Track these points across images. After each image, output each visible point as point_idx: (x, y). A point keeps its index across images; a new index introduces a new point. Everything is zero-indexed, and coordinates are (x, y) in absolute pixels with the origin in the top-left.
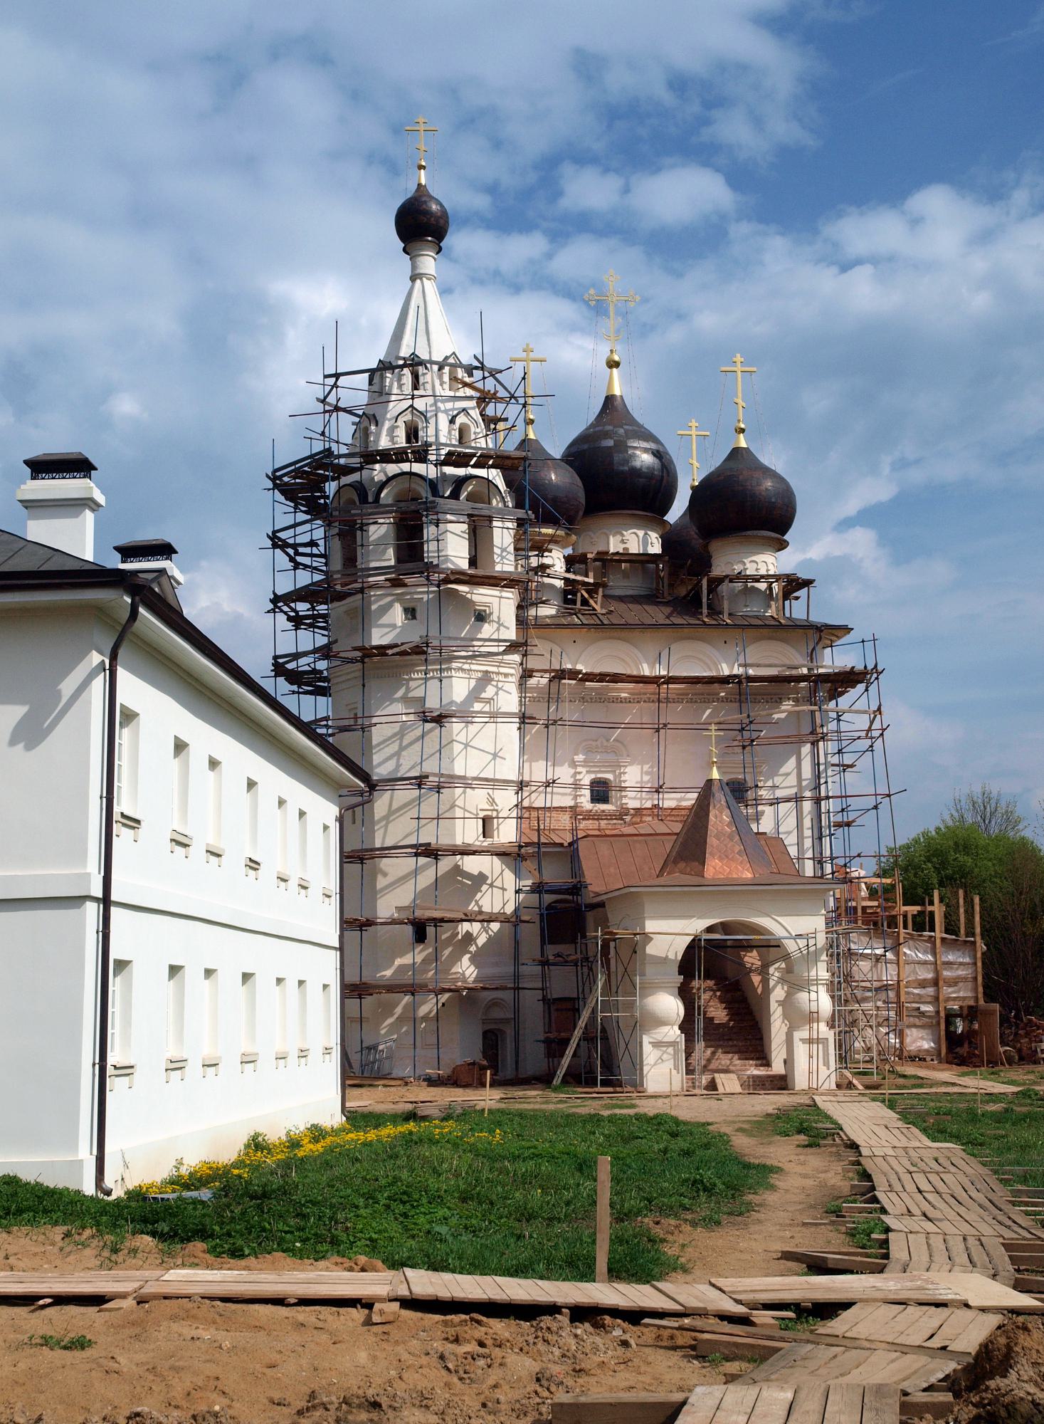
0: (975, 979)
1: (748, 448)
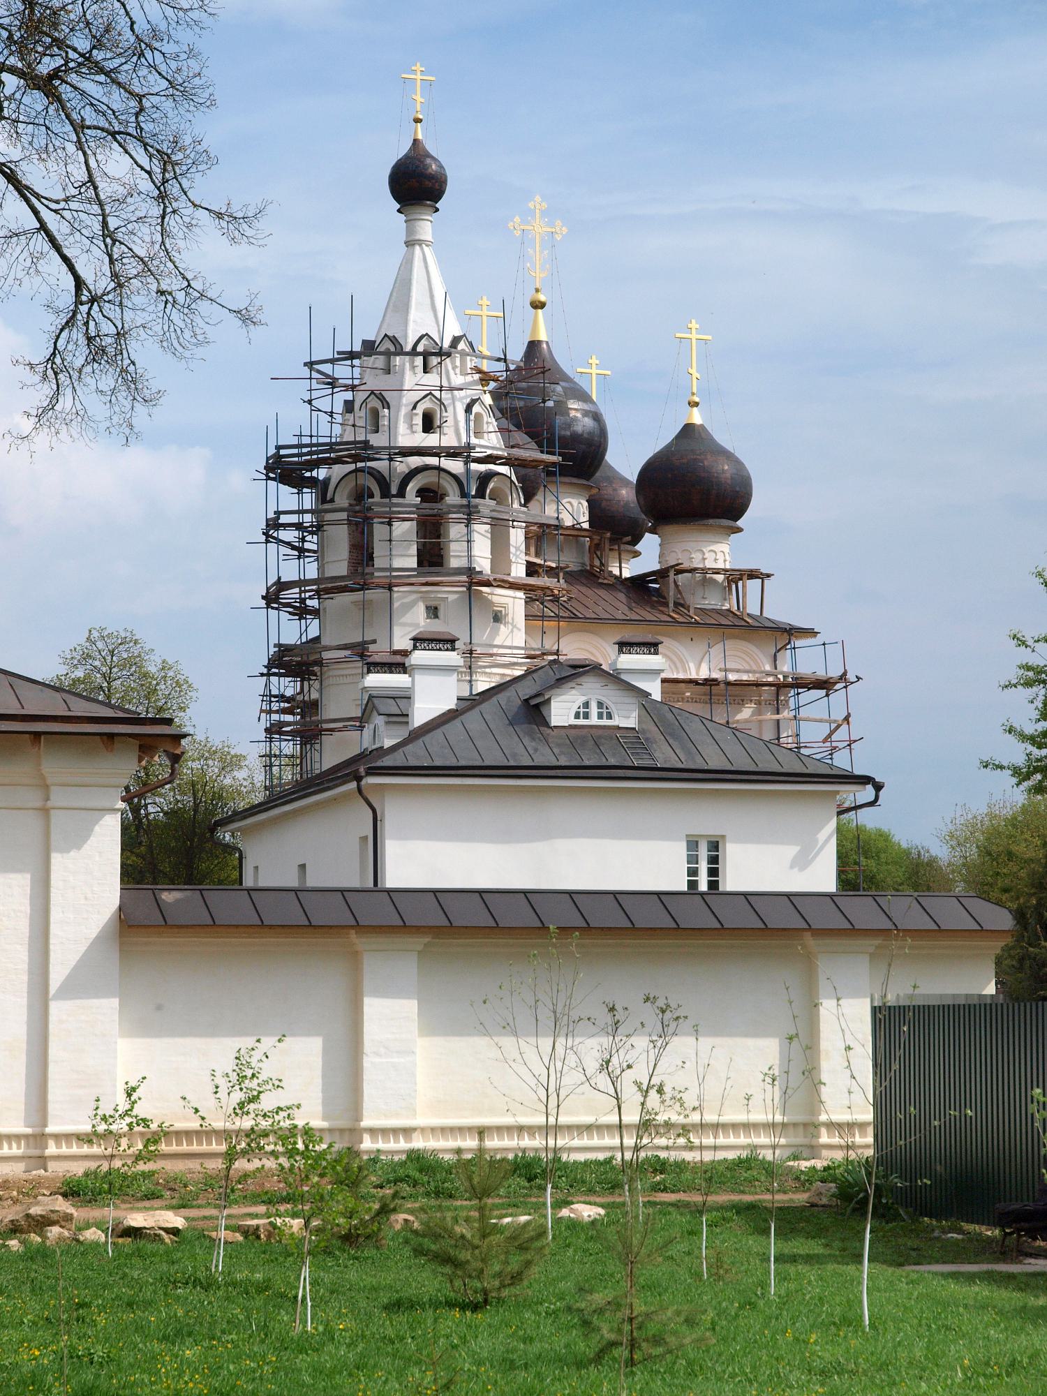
1: (702, 426)
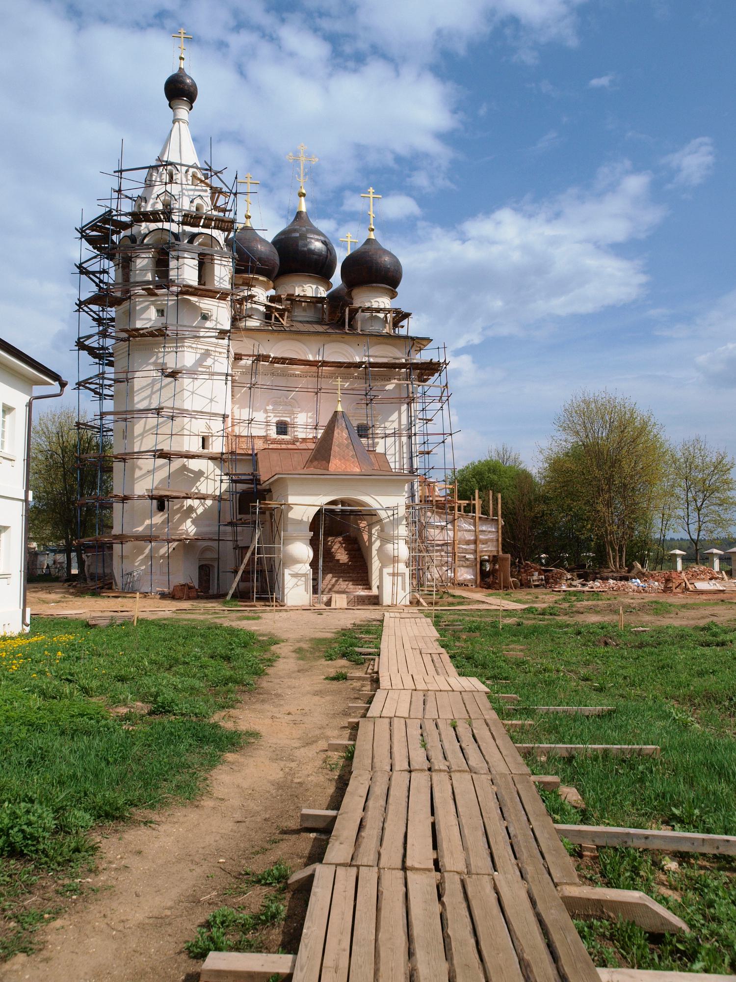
0: (498, 540)
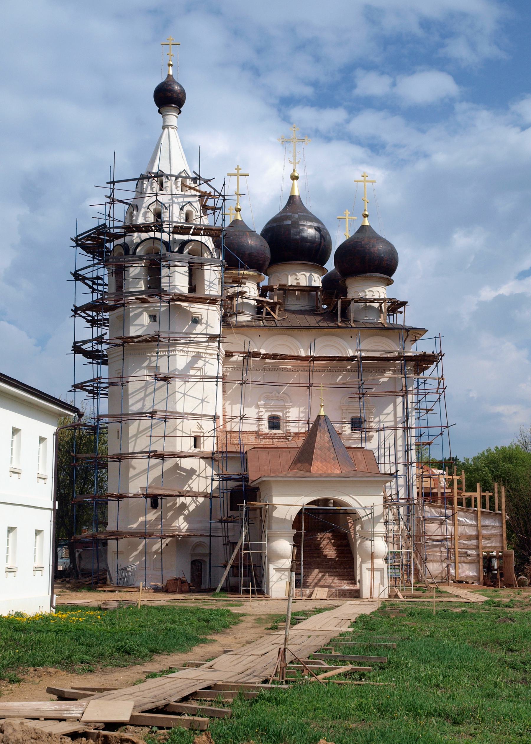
0: (502, 535)
1: (370, 226)
